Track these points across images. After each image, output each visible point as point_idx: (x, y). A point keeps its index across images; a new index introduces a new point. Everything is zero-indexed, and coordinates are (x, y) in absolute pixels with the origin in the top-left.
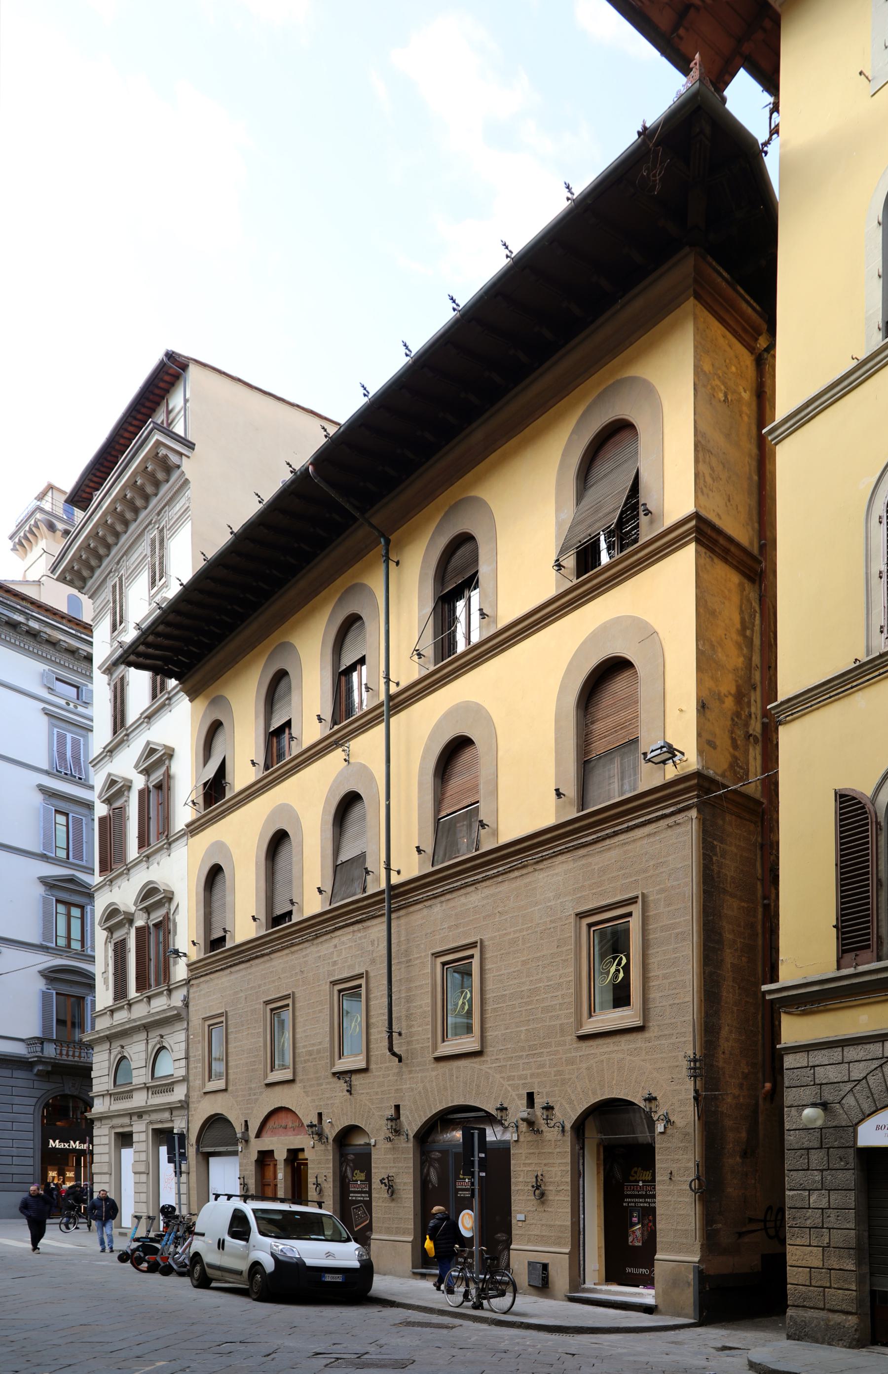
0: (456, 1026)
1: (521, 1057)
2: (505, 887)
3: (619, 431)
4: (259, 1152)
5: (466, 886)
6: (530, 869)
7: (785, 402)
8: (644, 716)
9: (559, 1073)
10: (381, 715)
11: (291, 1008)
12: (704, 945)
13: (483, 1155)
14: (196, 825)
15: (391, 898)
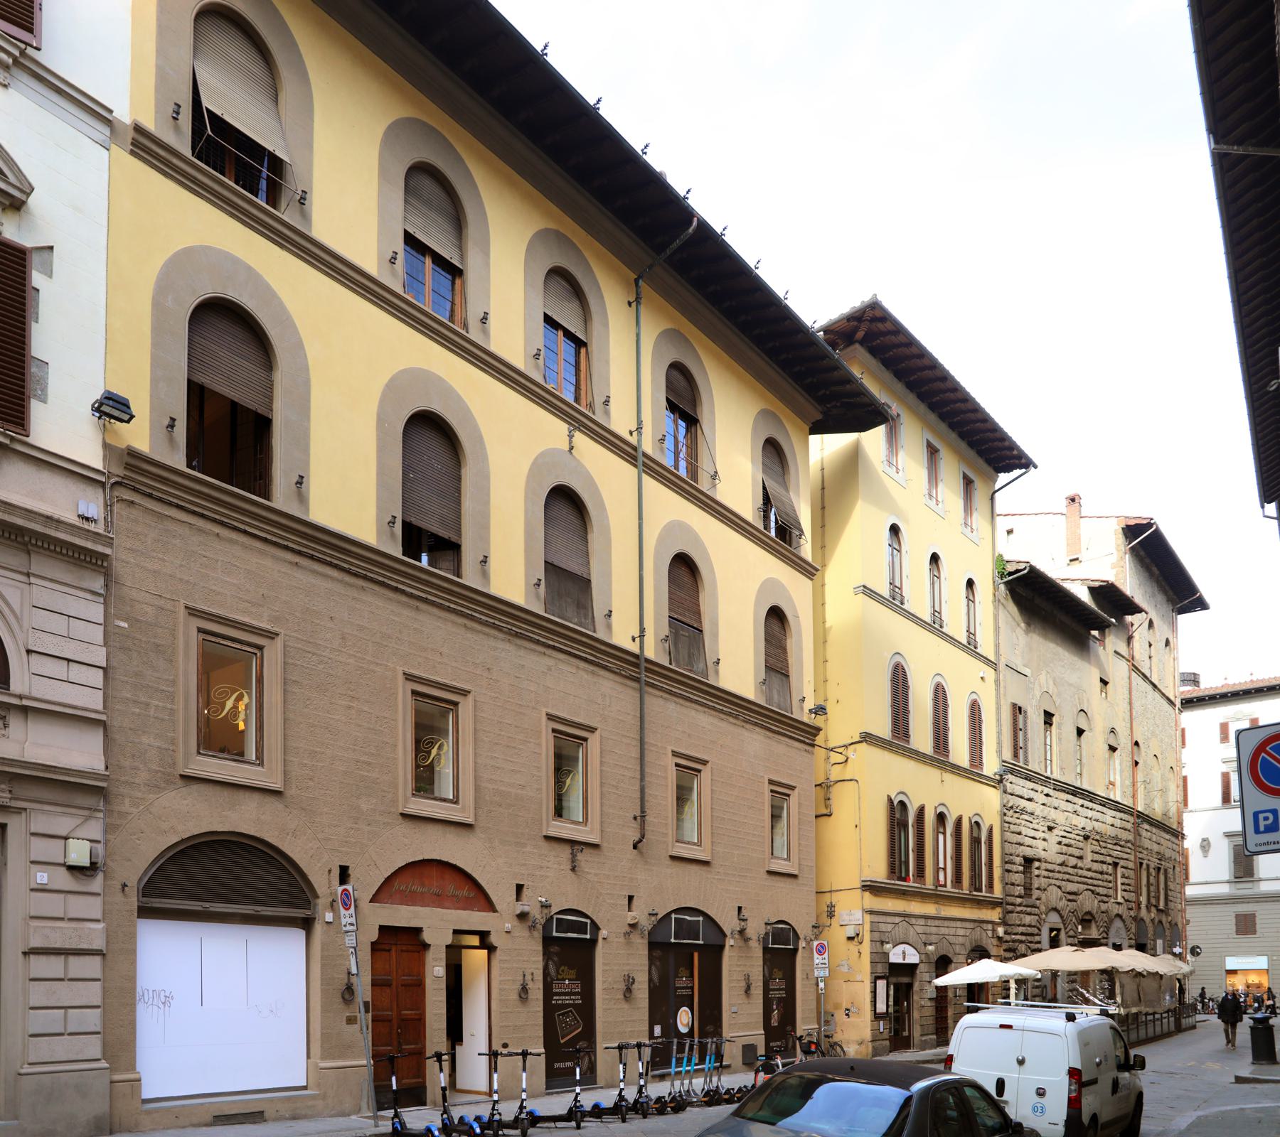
2: (723, 725)
4: (382, 928)
5: (713, 708)
14: (175, 161)
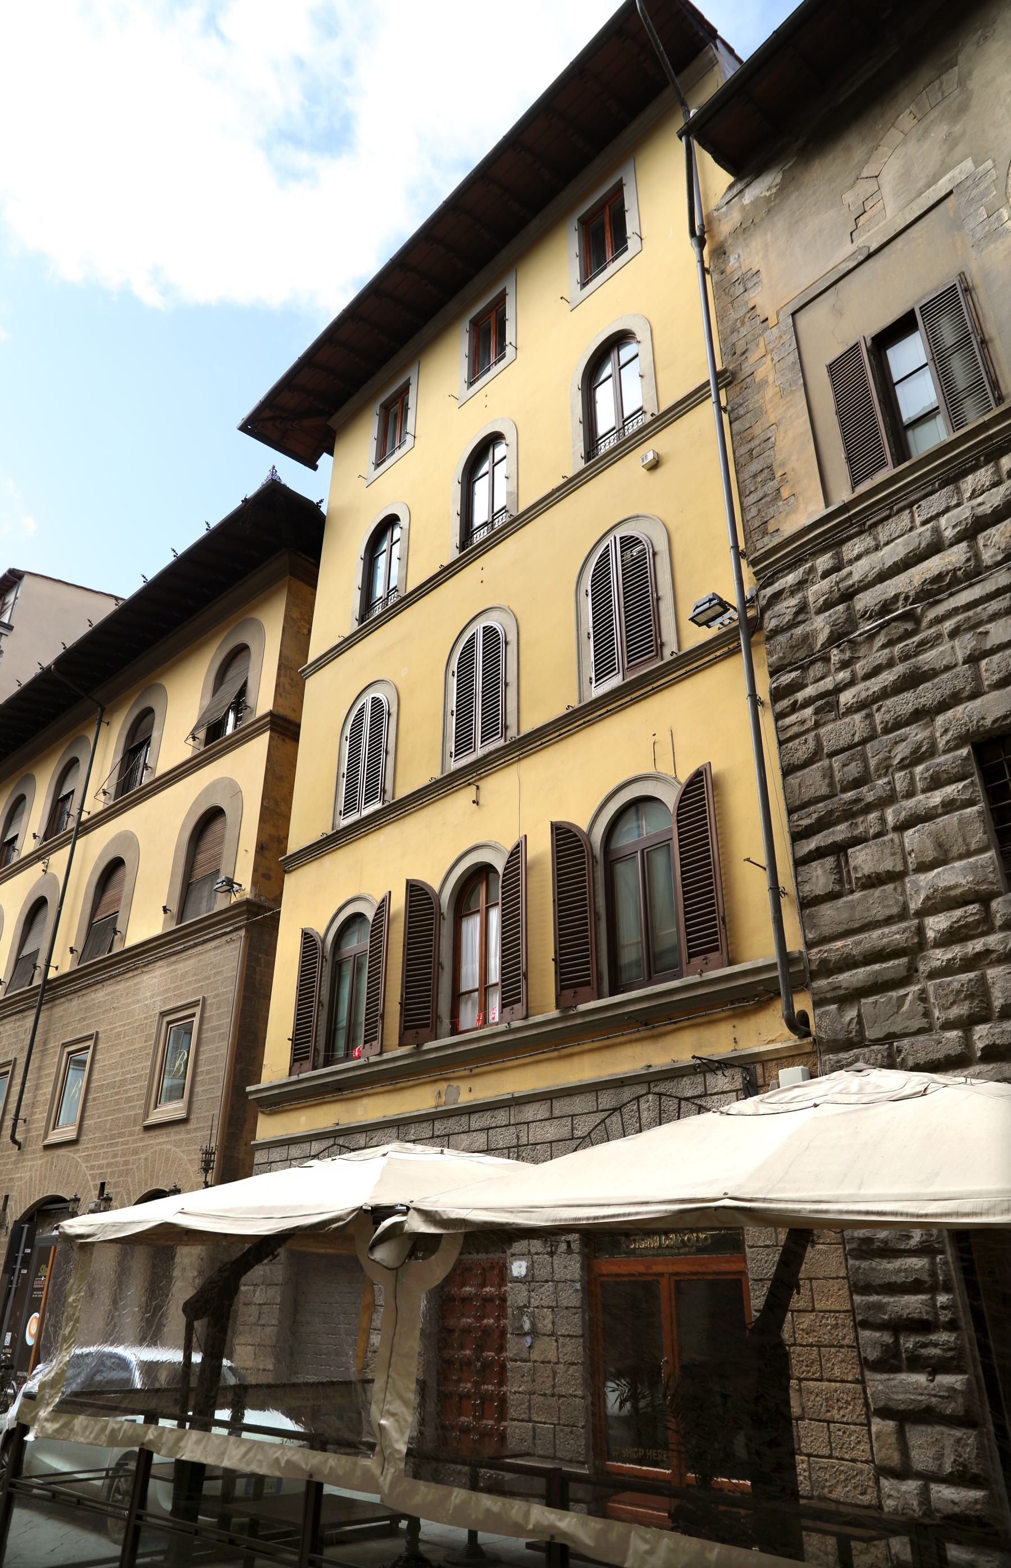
0: (171, 1089)
1: (102, 1146)
2: (122, 985)
3: (241, 651)
6: (139, 971)
7: (315, 652)
8: (225, 853)
9: (126, 1163)
10: (70, 838)
11: (90, 1051)
12: (238, 1044)
13: (28, 1251)
15: (44, 991)
